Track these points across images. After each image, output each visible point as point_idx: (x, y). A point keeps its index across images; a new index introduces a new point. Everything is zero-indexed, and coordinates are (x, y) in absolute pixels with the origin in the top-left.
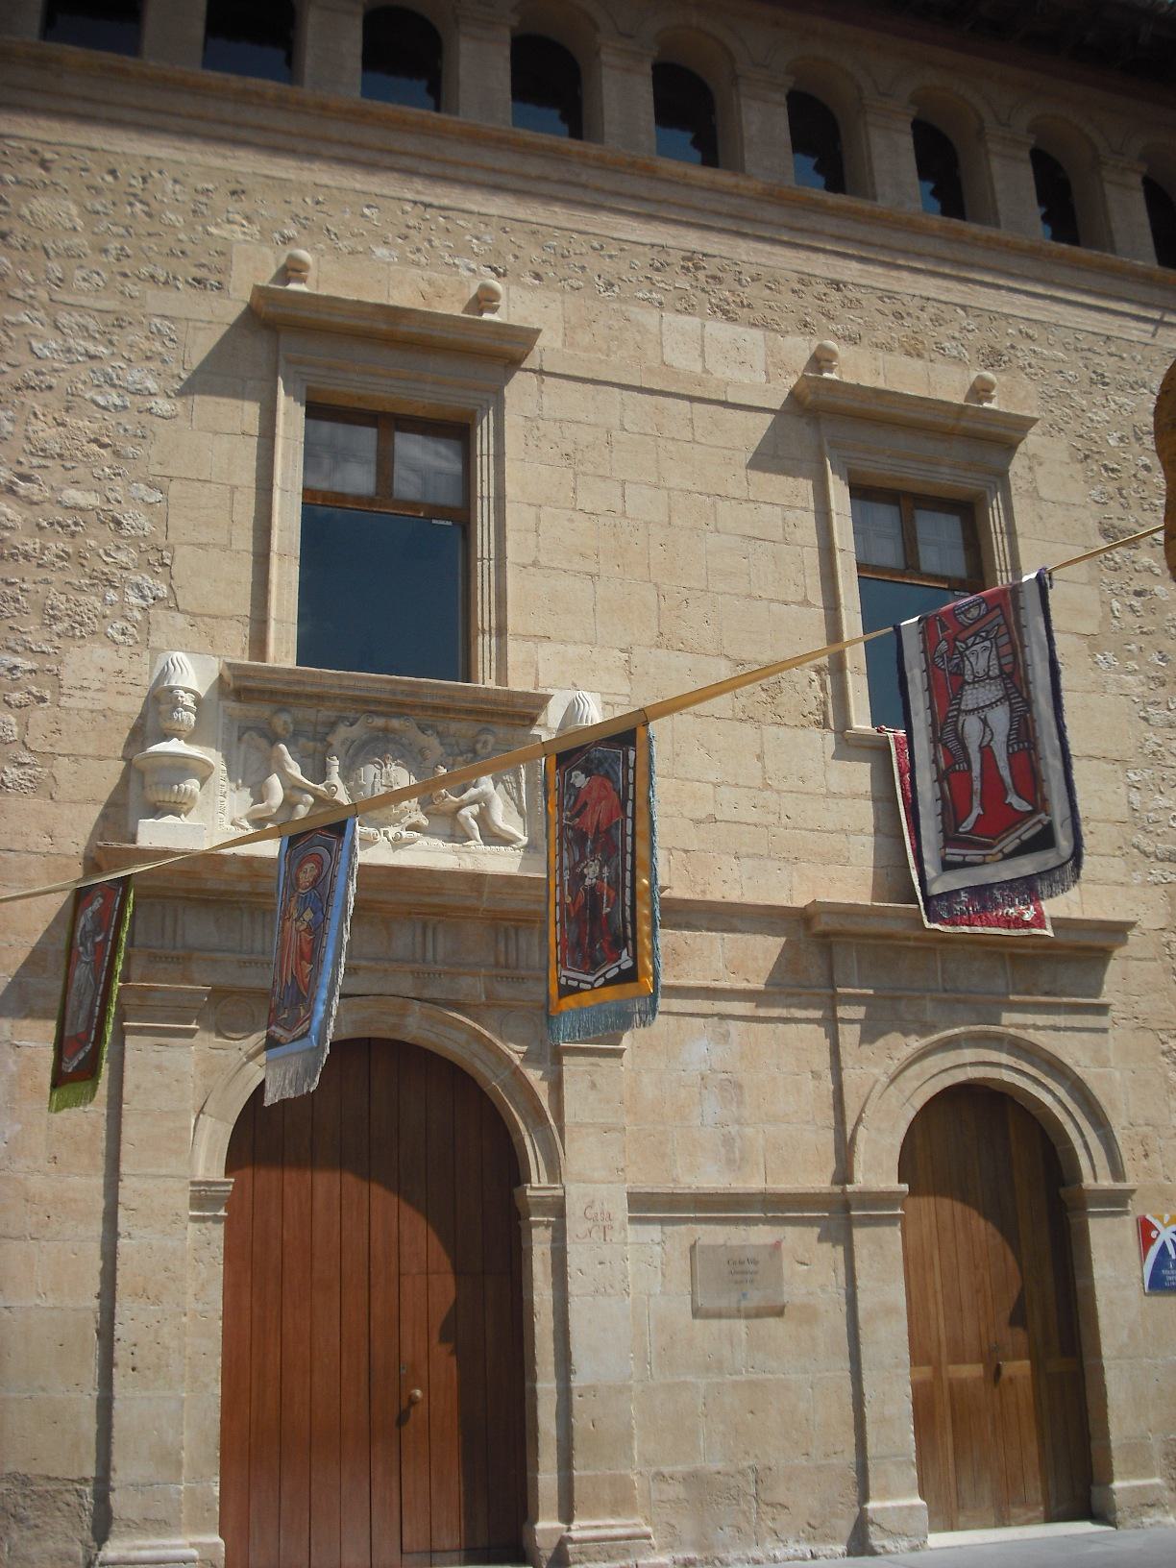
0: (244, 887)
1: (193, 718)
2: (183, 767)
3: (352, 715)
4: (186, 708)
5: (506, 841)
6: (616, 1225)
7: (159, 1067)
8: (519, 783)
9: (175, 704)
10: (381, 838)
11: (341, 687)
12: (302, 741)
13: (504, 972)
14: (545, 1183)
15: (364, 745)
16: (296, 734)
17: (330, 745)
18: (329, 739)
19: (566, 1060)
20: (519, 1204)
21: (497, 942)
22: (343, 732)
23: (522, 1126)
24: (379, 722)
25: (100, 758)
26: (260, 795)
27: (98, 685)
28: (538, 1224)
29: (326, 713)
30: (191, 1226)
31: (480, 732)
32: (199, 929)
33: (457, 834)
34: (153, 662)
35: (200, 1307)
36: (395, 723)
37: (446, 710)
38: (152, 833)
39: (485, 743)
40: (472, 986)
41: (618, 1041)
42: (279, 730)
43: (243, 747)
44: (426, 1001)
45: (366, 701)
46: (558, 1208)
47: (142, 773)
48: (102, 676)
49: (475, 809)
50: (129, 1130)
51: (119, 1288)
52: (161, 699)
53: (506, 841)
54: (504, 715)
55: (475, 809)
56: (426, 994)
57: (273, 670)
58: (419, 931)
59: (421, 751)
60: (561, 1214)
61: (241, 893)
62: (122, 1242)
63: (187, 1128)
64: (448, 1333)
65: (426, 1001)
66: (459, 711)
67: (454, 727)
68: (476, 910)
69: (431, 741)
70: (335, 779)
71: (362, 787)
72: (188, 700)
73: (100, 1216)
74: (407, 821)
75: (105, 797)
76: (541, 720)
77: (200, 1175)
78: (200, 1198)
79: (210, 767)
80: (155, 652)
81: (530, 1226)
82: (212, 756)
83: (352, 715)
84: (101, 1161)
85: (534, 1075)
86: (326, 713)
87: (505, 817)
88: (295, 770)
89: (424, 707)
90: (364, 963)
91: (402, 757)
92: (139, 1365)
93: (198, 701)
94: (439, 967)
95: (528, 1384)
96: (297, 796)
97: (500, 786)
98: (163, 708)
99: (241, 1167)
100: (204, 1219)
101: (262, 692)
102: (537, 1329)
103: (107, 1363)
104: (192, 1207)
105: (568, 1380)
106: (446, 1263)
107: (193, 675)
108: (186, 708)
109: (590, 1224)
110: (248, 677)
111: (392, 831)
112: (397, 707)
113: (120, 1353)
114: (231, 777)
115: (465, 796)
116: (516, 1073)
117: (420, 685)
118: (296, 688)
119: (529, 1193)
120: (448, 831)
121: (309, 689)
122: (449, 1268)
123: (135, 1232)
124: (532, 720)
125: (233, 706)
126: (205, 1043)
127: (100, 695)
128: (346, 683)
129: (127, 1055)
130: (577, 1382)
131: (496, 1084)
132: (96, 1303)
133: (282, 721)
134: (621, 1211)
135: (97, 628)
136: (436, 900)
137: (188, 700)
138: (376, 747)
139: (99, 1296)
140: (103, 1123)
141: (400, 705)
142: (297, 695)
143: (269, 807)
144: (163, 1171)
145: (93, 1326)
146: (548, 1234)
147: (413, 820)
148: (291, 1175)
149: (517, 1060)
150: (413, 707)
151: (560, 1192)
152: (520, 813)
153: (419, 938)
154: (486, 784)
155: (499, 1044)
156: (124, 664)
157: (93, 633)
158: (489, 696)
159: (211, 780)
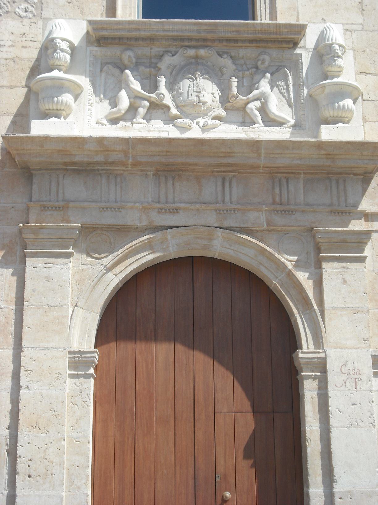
0: (100, 158)
1: (68, 57)
2: (60, 87)
3: (173, 49)
4: (62, 51)
5: (280, 123)
6: (364, 378)
7: (48, 278)
8: (288, 86)
9: (55, 48)
10: (194, 125)
11: (165, 30)
12: (142, 68)
13: (279, 207)
14: (312, 348)
15: (182, 68)
16: (137, 64)
17: (160, 69)
18: (159, 65)
19: (324, 265)
20: (296, 364)
21: (273, 187)
22: (168, 60)
23: (295, 311)
24: (191, 52)
25: (11, 87)
26: (114, 103)
27: (10, 43)
28: (309, 377)
29: (156, 50)
30: (68, 380)
31: (260, 54)
32: (73, 188)
33: (247, 121)
34: (45, 26)
35: (75, 435)
36: (202, 52)
37: (236, 41)
38: (39, 128)
39: (263, 61)
40: (258, 218)
41: (362, 251)
42: (126, 62)
43: (103, 75)
44: (227, 228)
45: (182, 39)
46: (322, 367)
47: (37, 94)
48: (12, 38)
49: (258, 104)
50: (28, 319)
51: (20, 422)
52: (49, 47)
53: (280, 123)
54: (275, 41)
55: (258, 104)
56: (226, 224)
57: (119, 23)
58: (220, 183)
59: (220, 70)
60: (323, 369)
61: (98, 163)
62: (22, 392)
63: (67, 316)
64: (250, 452)
65: (227, 228)
66: (244, 41)
67: (242, 52)
68: (258, 167)
69: (226, 62)
70: (163, 88)
71: (181, 94)
72: (64, 45)
73: (10, 375)
74: (212, 114)
75: (14, 111)
76: (301, 44)
77: (75, 347)
78: (75, 362)
79: (79, 86)
80: (46, 20)
81: (303, 378)
82: (84, 81)
83: (173, 49)
84: (11, 340)
85: (302, 276)
86: (156, 50)
87: (278, 106)
88: (136, 86)
89: (220, 40)
90: (182, 205)
91: (207, 73)
92: (33, 474)
93: (72, 47)
94: (234, 206)
95: (305, 489)
96: (138, 102)
97: (275, 89)
98: (50, 51)
99: (108, 342)
100: (77, 376)
101: (113, 39)
102: (309, 450)
103: (13, 472)
104: (70, 368)
105: (332, 487)
106: (247, 404)
107: (70, 31)
108: (62, 51)
109: (345, 377)
110: (103, 29)
111: (202, 121)
112: (203, 42)
113: (21, 465)
114: (96, 93)
115: (251, 96)
116: (290, 274)
117: (216, 25)
118: (134, 34)
119: (300, 355)
120: (241, 120)
121: (143, 34)
122: (250, 409)
123: (32, 386)
124: (295, 44)
125: (96, 50)
126: (78, 261)
127: (11, 49)
128: (166, 27)
129: (27, 270)
130: (338, 488)
131: (275, 283)
132: (7, 432)
133: (128, 56)
134: (367, 368)
135: (10, 9)
136: (230, 161)
137: (64, 45)
138: (192, 67)
139: (9, 428)
140: (12, 315)
141: (205, 40)
142: (136, 39)
143: (120, 110)
144: (50, 345)
145: (5, 447)
146: (315, 384)
147: (214, 114)
148: (141, 346)
149: (290, 266)
150: (213, 41)
151: (322, 355)
152: (290, 105)
153: (220, 188)
154: (264, 86)
155: (277, 255)
156: (26, 29)
157: (7, 12)
158: (264, 29)
159: (82, 96)
